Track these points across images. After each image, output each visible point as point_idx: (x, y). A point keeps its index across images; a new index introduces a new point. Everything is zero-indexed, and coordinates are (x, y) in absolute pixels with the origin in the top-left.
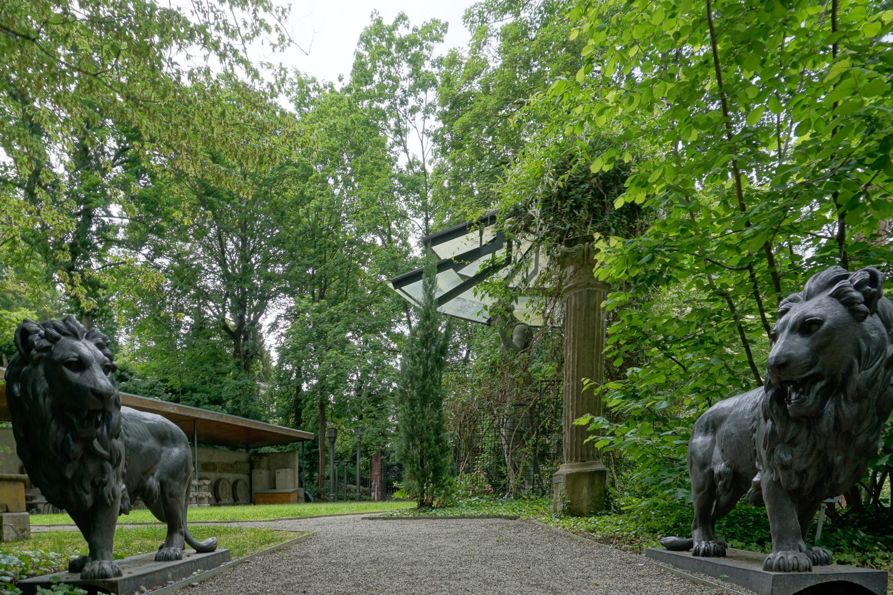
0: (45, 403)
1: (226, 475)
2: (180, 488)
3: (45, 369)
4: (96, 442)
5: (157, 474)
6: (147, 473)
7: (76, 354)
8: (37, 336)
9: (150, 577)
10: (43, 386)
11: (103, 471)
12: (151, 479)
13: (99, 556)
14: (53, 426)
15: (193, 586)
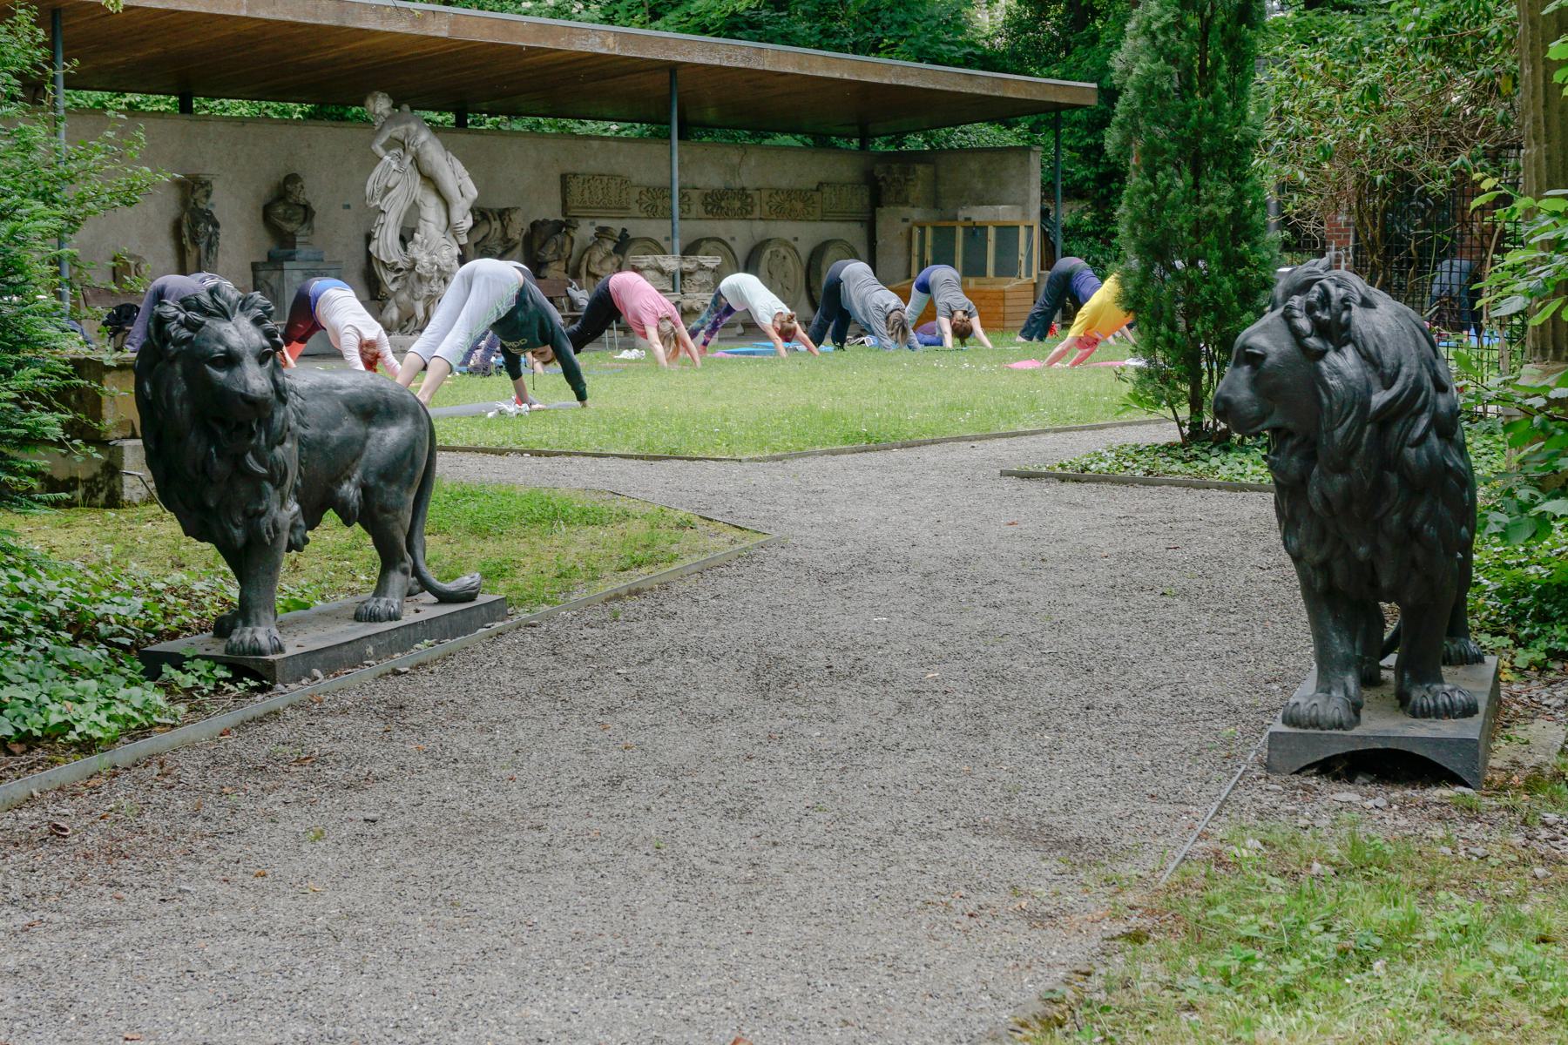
0: (182, 410)
1: (784, 229)
2: (399, 496)
3: (184, 366)
4: (249, 456)
5: (356, 477)
6: (339, 477)
7: (222, 348)
8: (174, 325)
9: (331, 654)
10: (180, 389)
11: (259, 495)
12: (345, 487)
13: (252, 618)
14: (192, 438)
15: (399, 673)
